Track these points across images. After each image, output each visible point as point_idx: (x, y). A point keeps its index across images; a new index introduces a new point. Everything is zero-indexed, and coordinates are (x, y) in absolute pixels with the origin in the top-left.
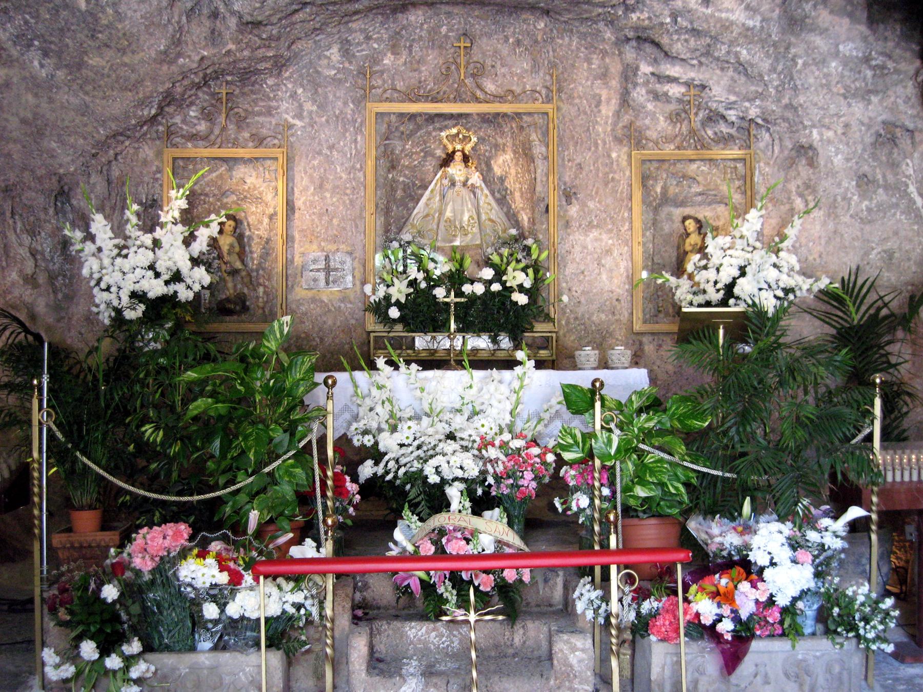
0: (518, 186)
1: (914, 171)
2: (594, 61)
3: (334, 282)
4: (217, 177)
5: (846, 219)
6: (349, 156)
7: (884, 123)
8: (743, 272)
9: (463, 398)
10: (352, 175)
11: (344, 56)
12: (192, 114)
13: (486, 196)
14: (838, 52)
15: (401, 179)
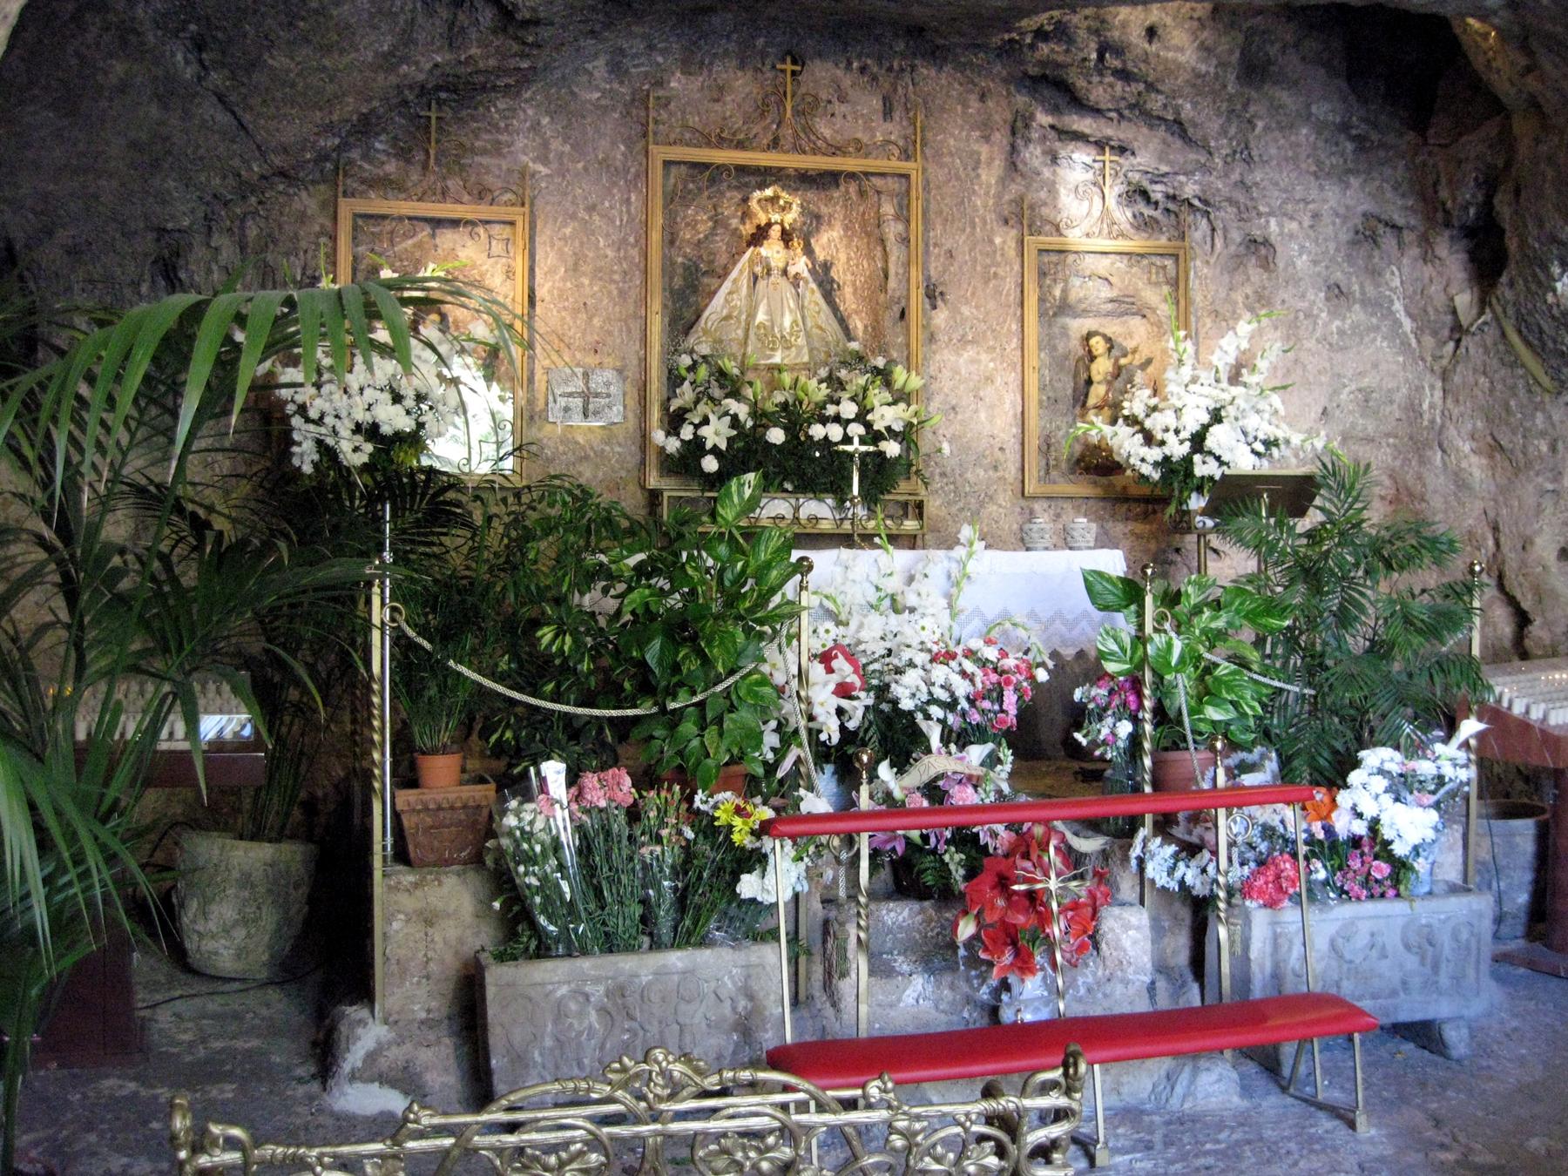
0: (849, 277)
1: (1402, 282)
3: (596, 413)
4: (414, 246)
5: (1310, 344)
7: (1364, 215)
8: (1216, 417)
9: (878, 589)
12: (378, 145)
13: (813, 292)
14: (1310, 115)
15: (680, 260)
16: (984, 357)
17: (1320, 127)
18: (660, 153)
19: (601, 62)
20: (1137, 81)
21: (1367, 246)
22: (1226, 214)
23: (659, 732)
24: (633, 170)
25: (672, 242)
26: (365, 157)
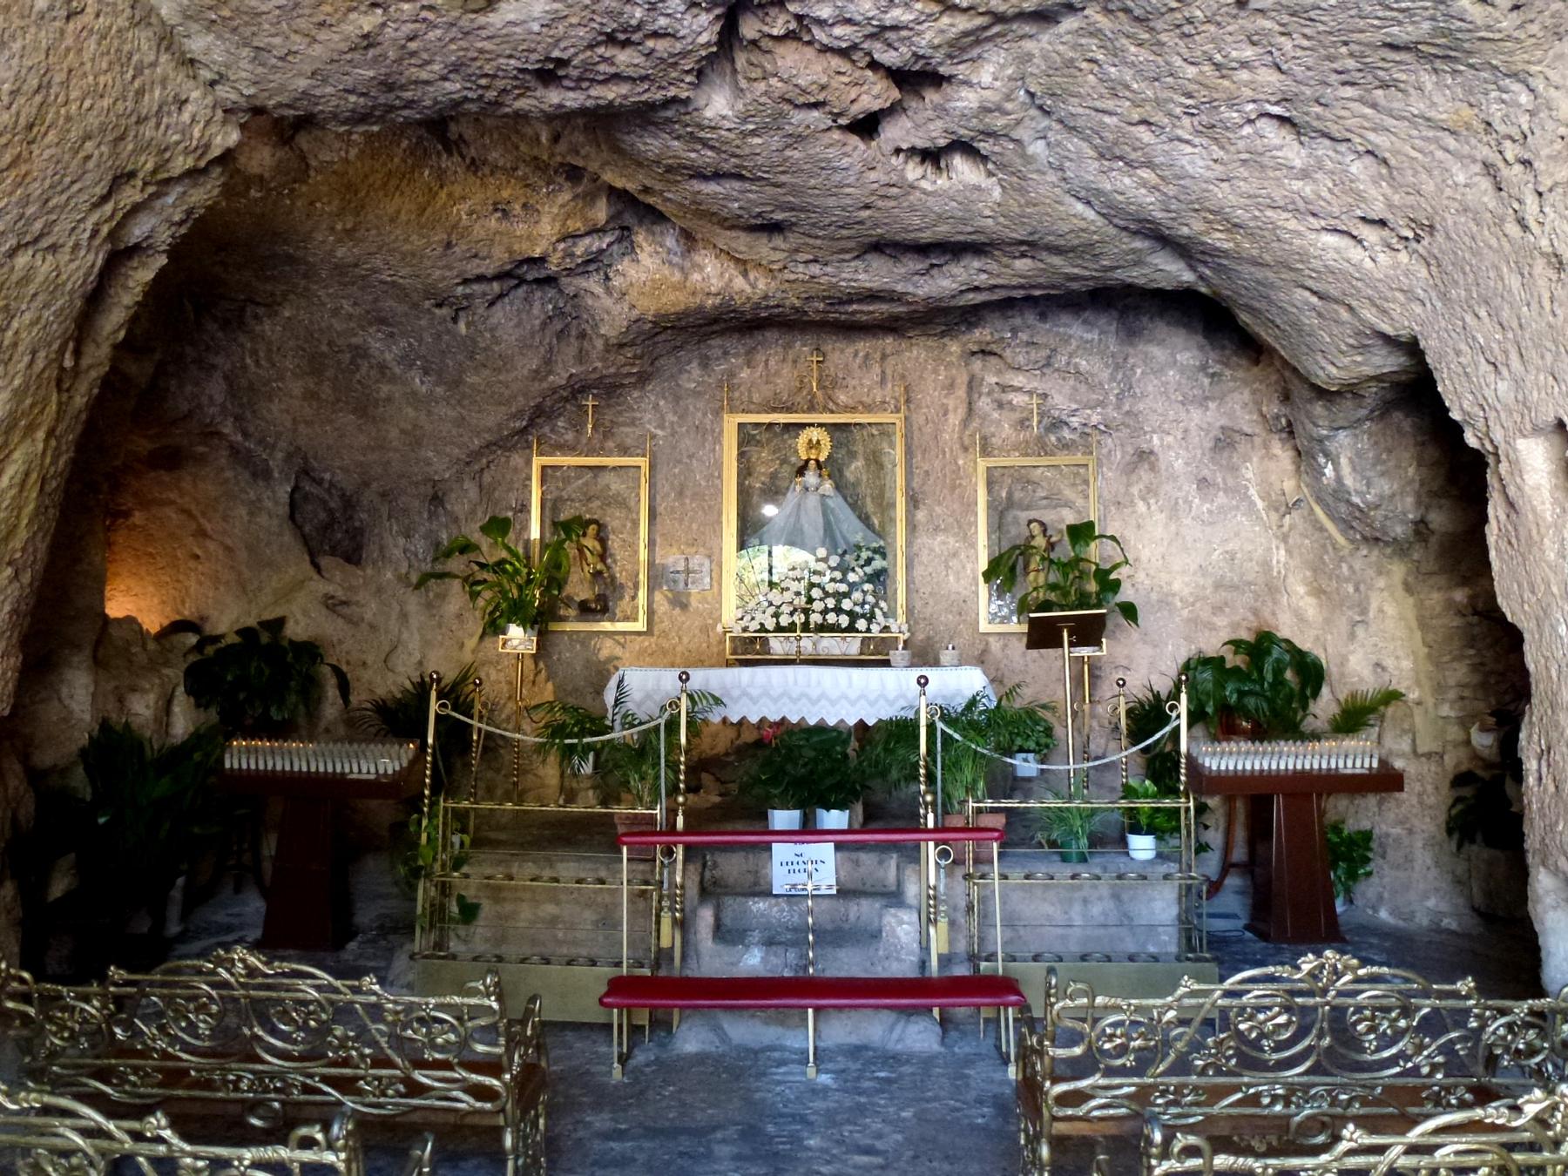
5: (1188, 521)
14: (1175, 362)
19: (694, 364)
26: (552, 431)
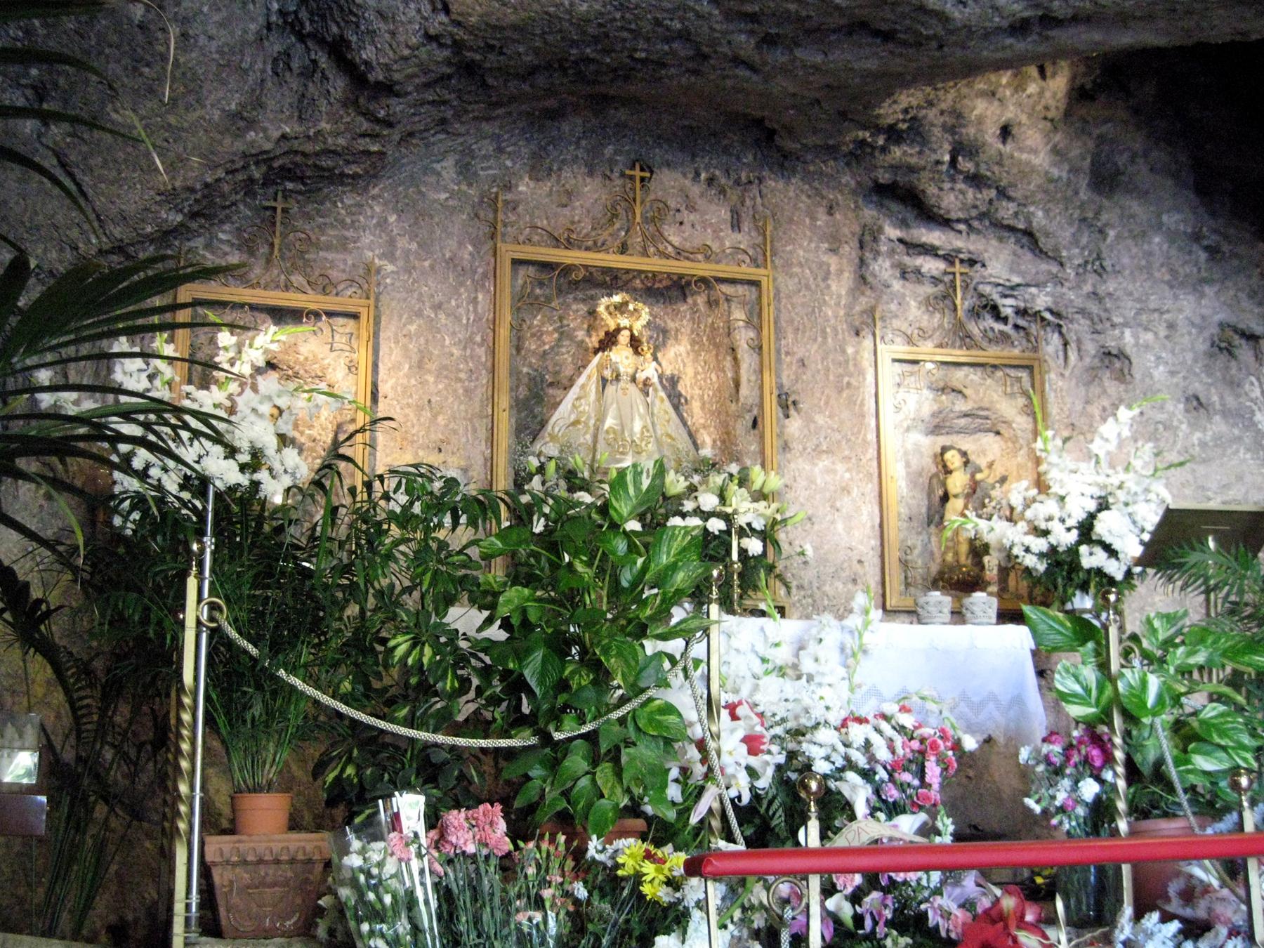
0: (697, 391)
2: (819, 216)
6: (464, 321)
10: (468, 351)
11: (461, 173)
12: (222, 236)
13: (662, 400)
15: (525, 370)
16: (840, 467)
17: (1172, 237)
18: (509, 251)
19: (450, 162)
20: (989, 187)
21: (1223, 357)
22: (1078, 328)
23: (537, 772)
24: (480, 270)
25: (518, 349)
26: (208, 246)
